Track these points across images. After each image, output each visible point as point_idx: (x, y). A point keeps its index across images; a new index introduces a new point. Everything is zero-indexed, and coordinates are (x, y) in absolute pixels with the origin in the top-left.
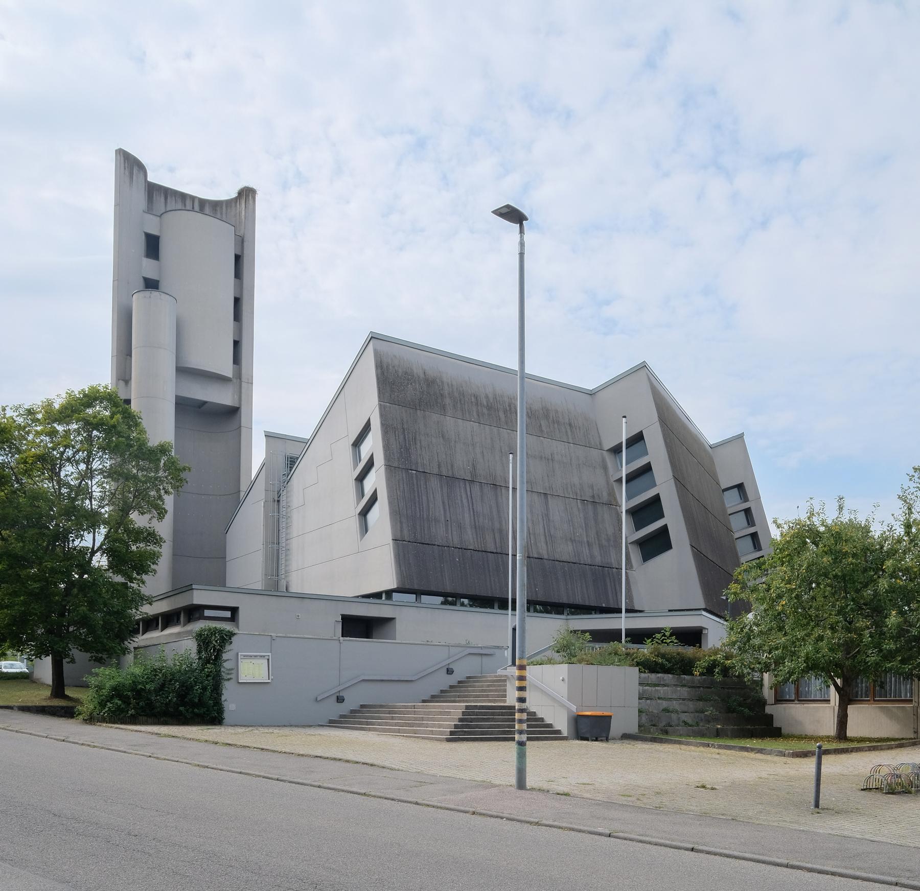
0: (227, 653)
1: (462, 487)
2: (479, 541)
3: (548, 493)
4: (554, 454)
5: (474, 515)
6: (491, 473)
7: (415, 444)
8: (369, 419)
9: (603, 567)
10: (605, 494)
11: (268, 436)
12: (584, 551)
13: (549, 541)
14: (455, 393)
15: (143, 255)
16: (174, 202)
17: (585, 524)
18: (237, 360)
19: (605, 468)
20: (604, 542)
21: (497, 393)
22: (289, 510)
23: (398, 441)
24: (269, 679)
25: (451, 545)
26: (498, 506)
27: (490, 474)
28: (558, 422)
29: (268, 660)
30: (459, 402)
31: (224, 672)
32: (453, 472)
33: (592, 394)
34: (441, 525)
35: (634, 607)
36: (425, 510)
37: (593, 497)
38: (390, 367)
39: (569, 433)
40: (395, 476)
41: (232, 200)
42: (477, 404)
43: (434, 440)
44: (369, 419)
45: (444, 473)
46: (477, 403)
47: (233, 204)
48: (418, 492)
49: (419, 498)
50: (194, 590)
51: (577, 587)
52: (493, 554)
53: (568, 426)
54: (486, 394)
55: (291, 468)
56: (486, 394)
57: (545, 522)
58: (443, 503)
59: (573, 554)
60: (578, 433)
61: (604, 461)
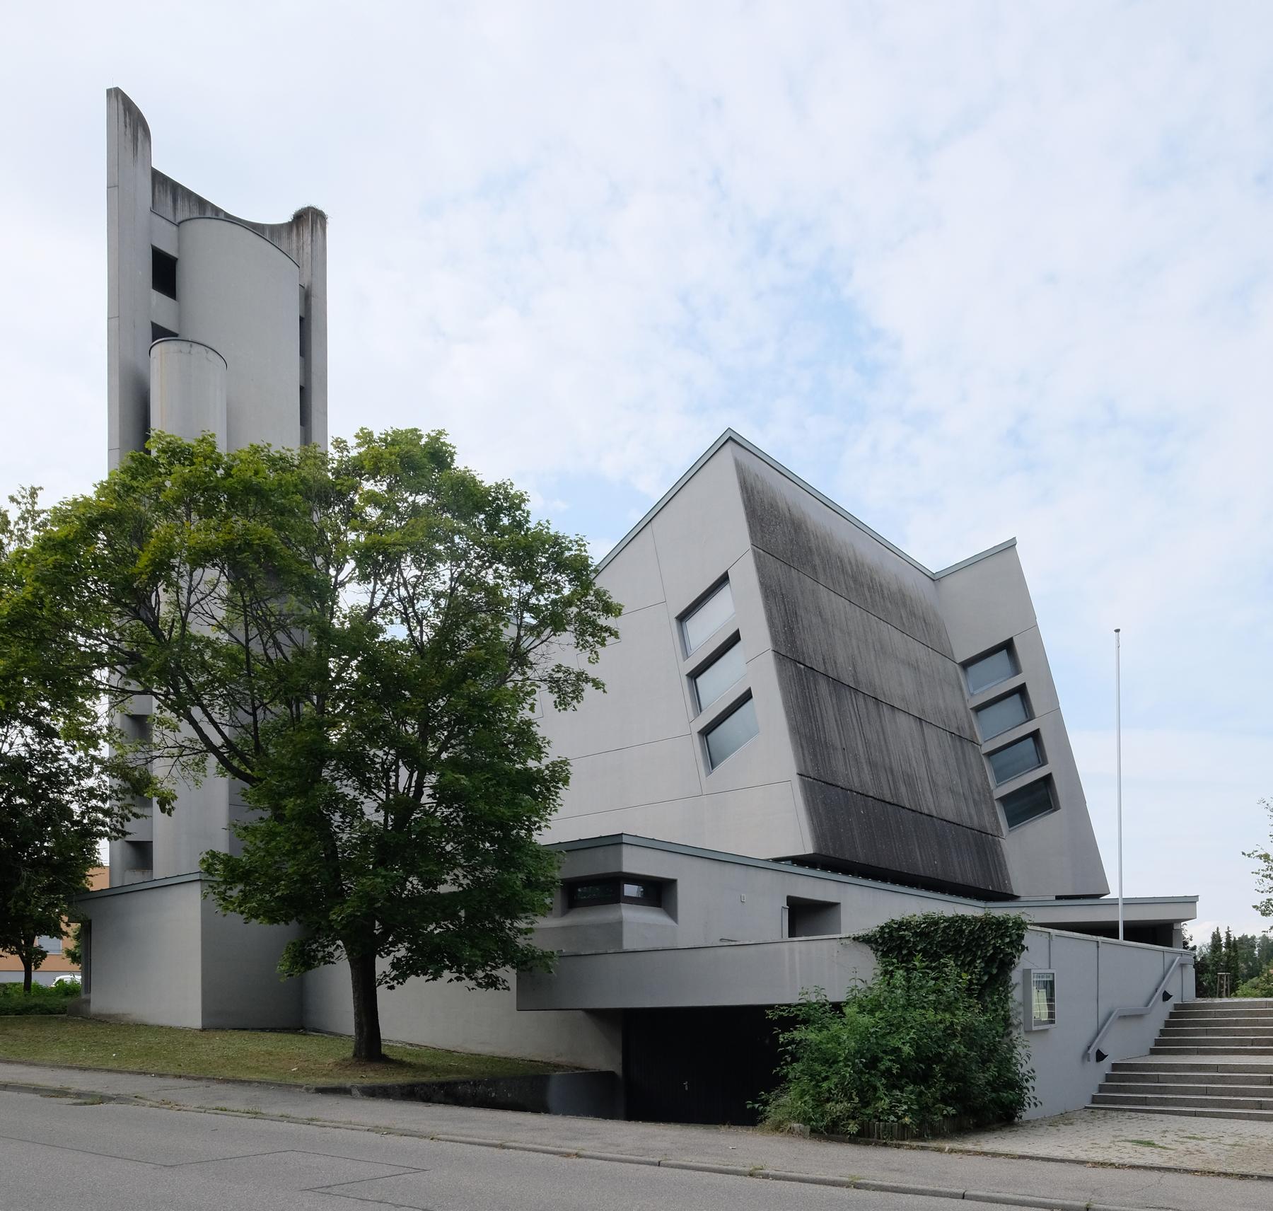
16: (187, 208)
26: (884, 733)
33: (935, 579)
35: (1012, 891)
41: (282, 226)
46: (844, 571)
50: (624, 846)
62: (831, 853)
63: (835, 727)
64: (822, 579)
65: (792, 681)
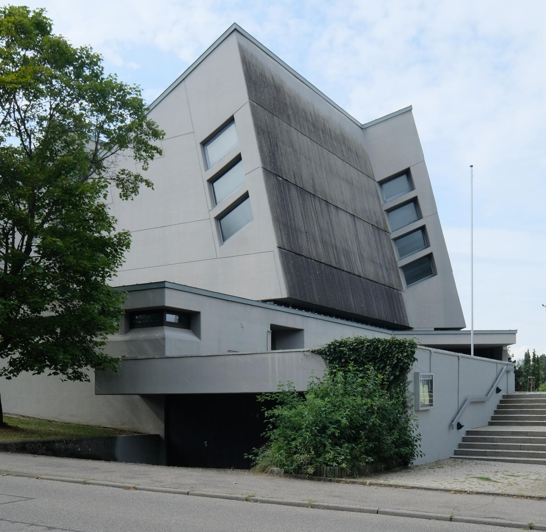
33: (363, 128)
46: (307, 120)
48: (286, 199)
57: (288, 195)
58: (302, 214)
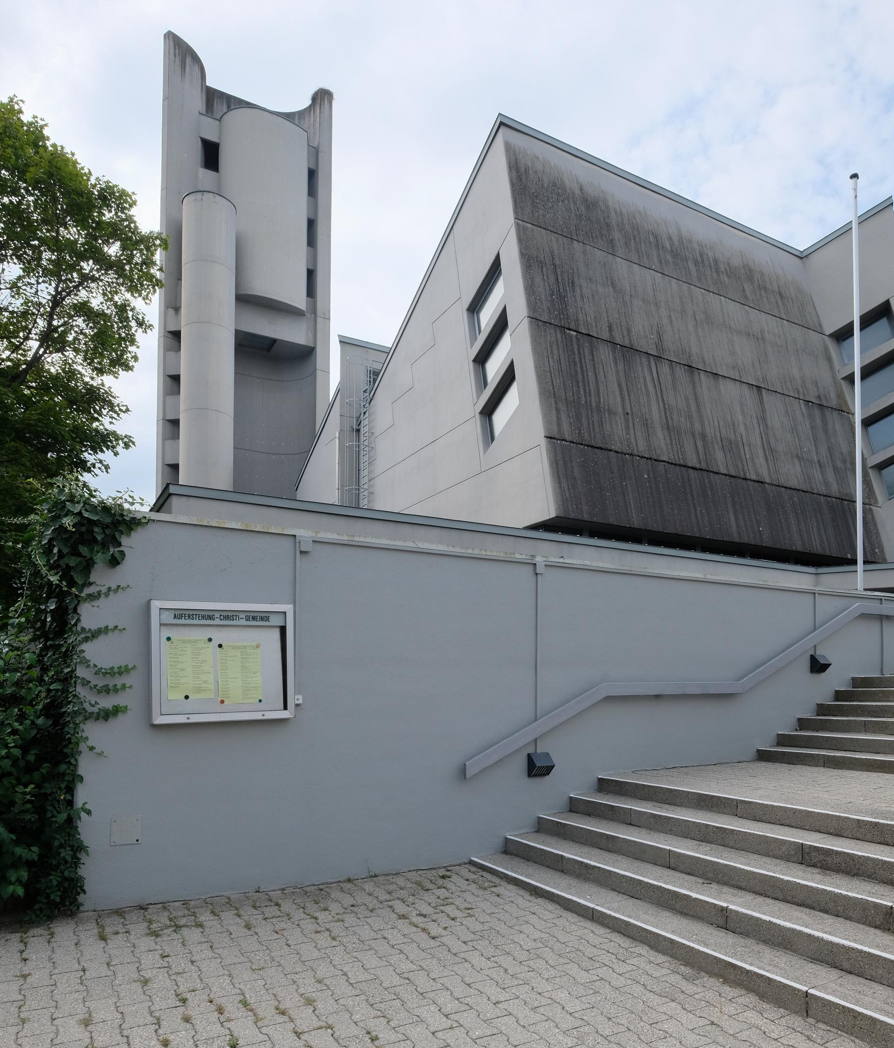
0: (102, 602)
1: (645, 366)
2: (675, 448)
3: (762, 386)
4: (764, 331)
5: (665, 409)
6: (684, 349)
7: (574, 289)
8: (498, 256)
9: (842, 499)
10: (833, 395)
11: (345, 342)
12: (816, 475)
13: (770, 457)
14: (627, 227)
15: (199, 165)
17: (813, 434)
18: (311, 291)
19: (829, 359)
20: (839, 464)
21: (684, 236)
22: (372, 439)
23: (546, 284)
24: (285, 708)
25: (636, 452)
26: (696, 399)
27: (682, 349)
28: (765, 289)
29: (283, 630)
30: (632, 238)
31: (85, 683)
32: (630, 341)
33: (802, 257)
34: (619, 419)
36: (592, 393)
37: (819, 397)
38: (531, 172)
39: (781, 304)
40: (545, 336)
42: (657, 246)
43: (601, 289)
44: (498, 256)
45: (618, 340)
46: (658, 245)
47: (307, 115)
49: (583, 375)
51: (812, 528)
52: (696, 471)
53: (778, 295)
54: (668, 234)
55: (375, 381)
56: (668, 234)
57: (762, 428)
58: (620, 386)
59: (802, 478)
60: (792, 307)
61: (826, 349)
62: (586, 517)
63: (617, 393)
64: (620, 252)
65: (555, 348)
